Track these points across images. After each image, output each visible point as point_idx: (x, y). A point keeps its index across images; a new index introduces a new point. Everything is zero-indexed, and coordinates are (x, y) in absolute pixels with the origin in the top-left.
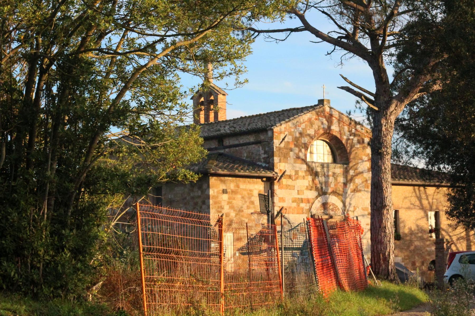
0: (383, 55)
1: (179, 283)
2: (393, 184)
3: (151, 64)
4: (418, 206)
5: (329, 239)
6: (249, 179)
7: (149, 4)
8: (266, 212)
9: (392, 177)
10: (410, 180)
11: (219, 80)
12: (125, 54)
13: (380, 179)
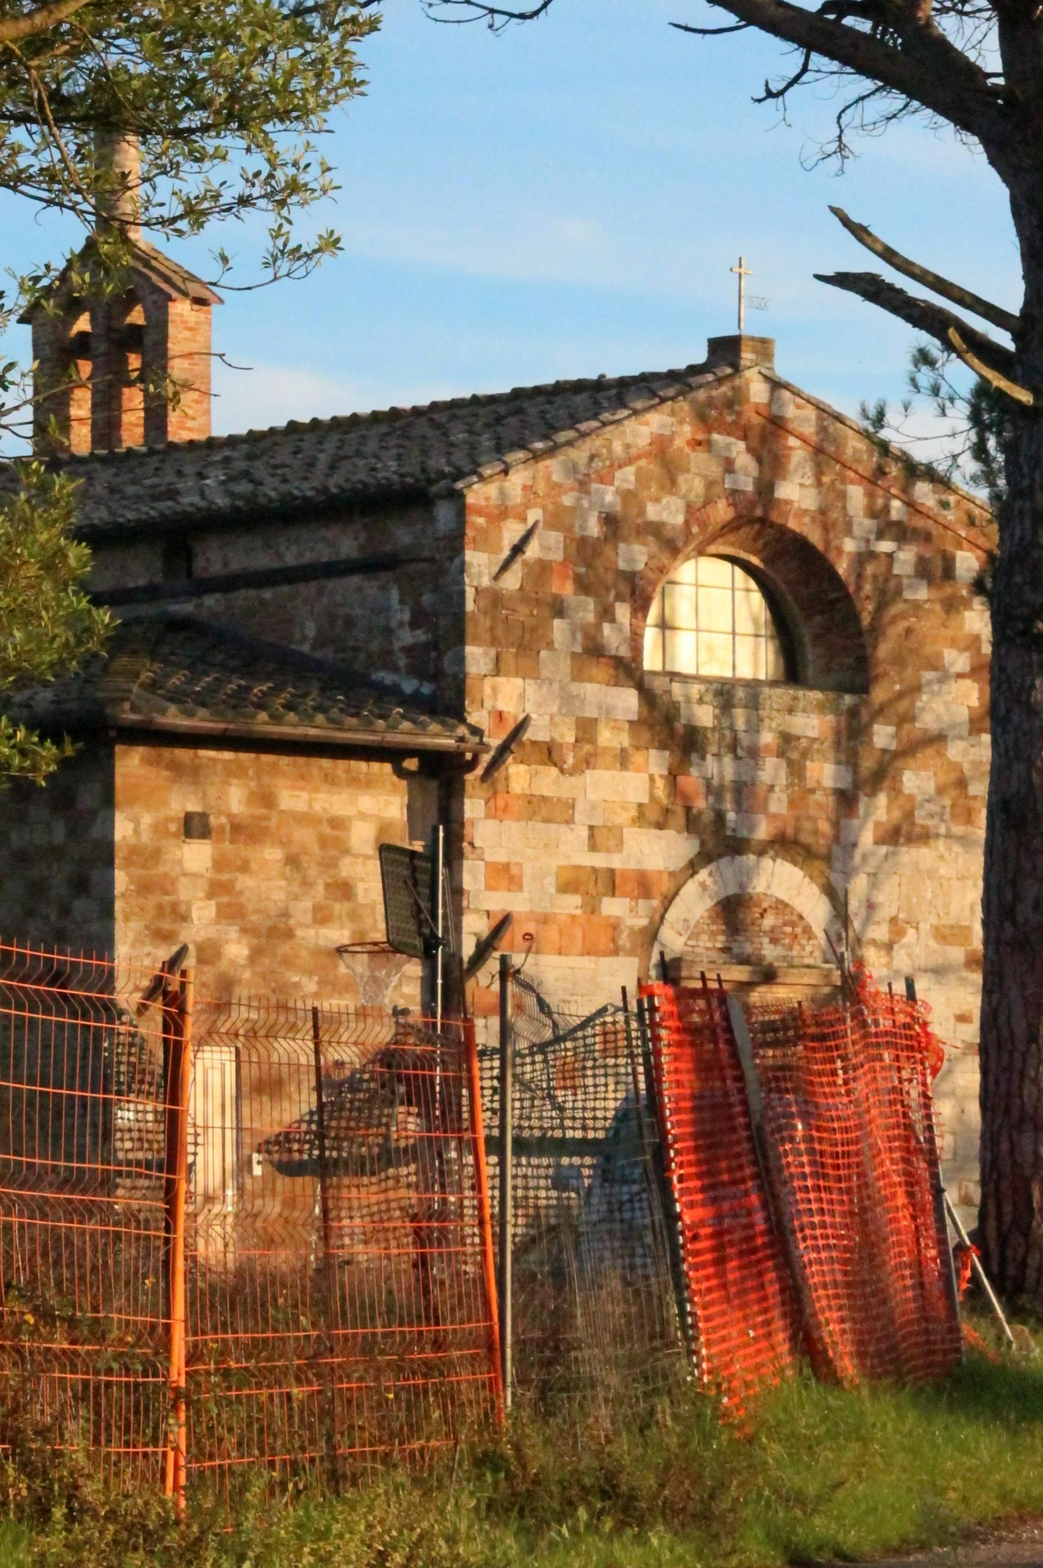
5: (756, 1097)
6: (325, 763)
8: (418, 942)
11: (180, 233)
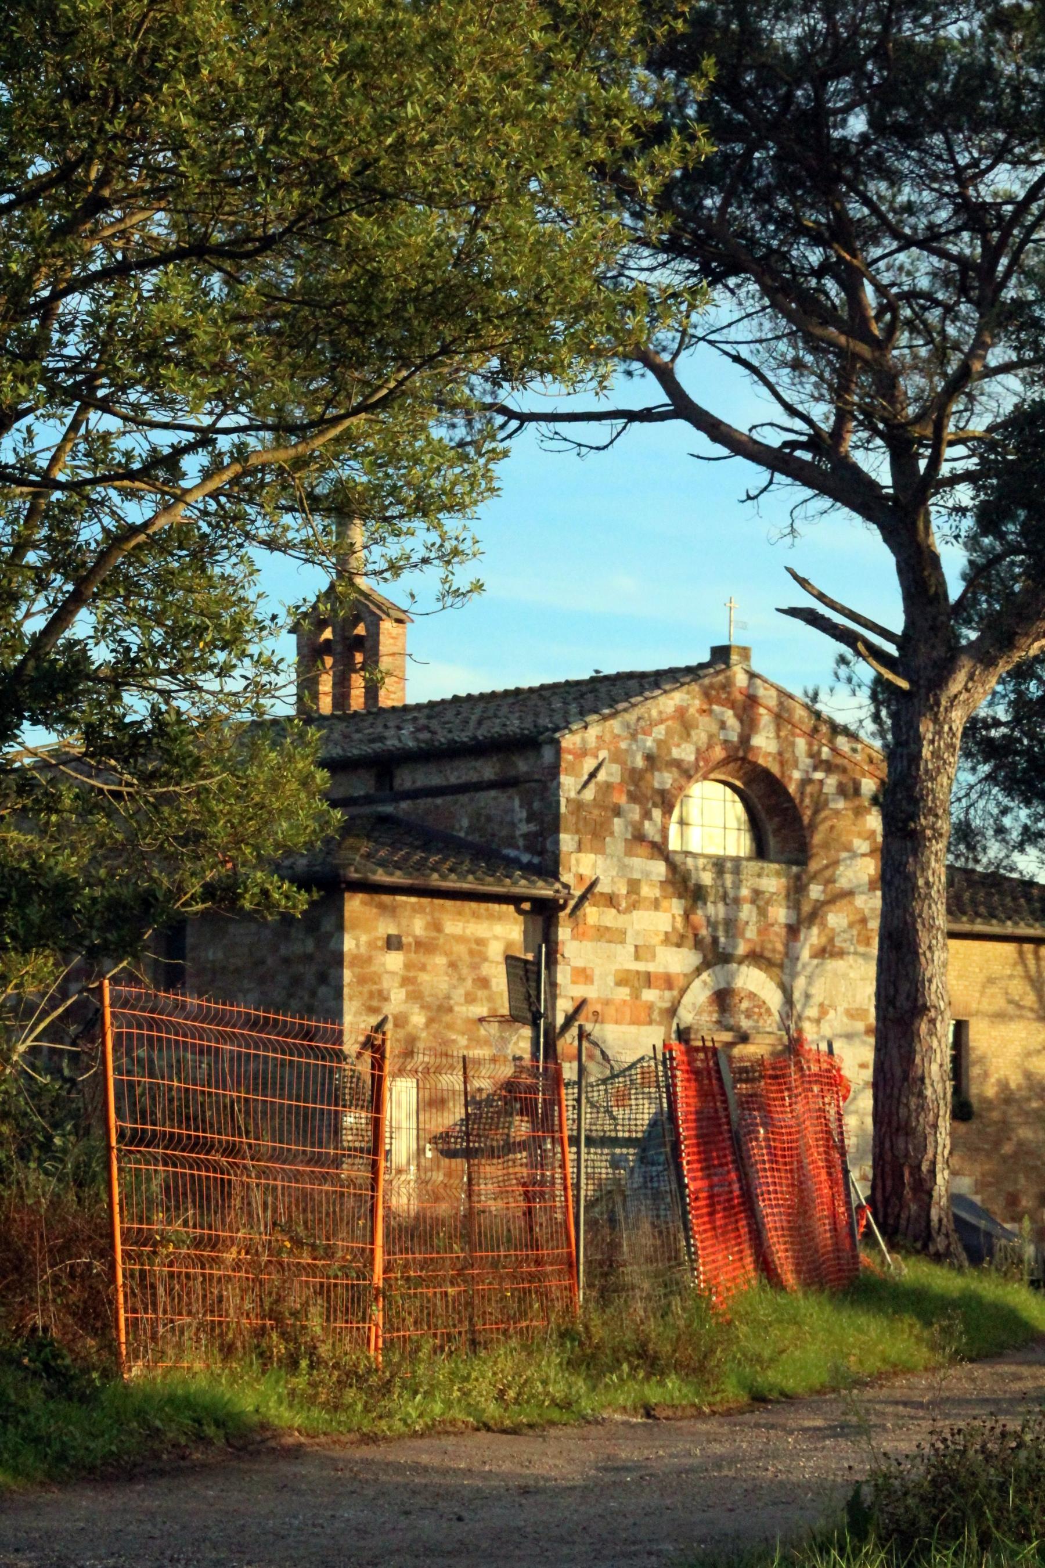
0: (933, 509)
1: (234, 1249)
2: (953, 935)
3: (163, 523)
4: (1032, 1010)
6: (473, 905)
7: (163, 324)
8: (529, 1016)
9: (949, 912)
10: (1009, 923)
11: (386, 580)
12: (75, 486)
13: (909, 919)
